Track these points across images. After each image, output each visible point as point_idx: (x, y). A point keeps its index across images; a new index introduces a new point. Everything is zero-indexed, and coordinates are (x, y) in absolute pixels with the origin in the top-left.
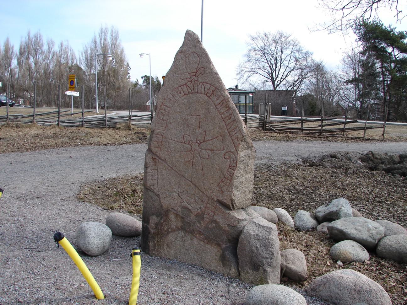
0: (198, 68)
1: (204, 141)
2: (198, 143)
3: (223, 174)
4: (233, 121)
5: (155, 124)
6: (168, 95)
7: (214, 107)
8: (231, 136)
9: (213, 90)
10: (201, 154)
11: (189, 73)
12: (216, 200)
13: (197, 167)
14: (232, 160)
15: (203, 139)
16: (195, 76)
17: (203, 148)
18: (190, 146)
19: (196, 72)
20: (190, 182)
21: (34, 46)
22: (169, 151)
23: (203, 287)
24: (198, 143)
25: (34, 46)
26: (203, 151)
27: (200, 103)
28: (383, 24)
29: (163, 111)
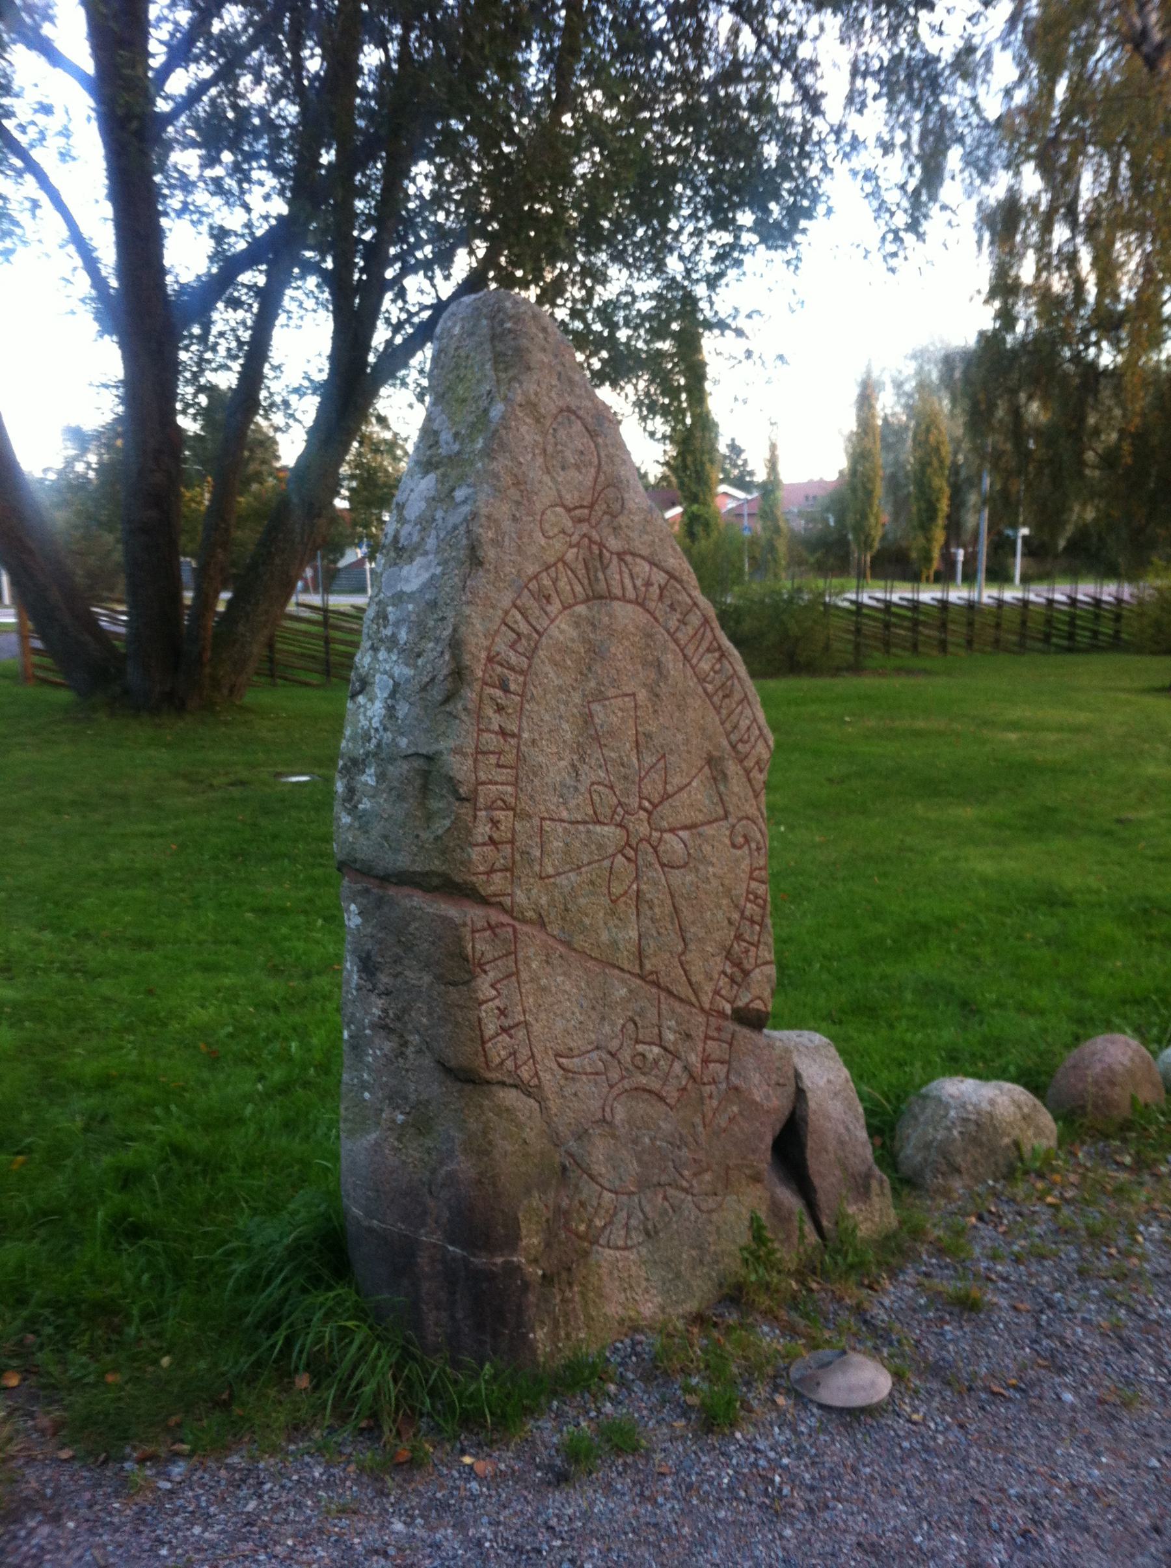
0: (599, 488)
1: (666, 797)
2: (645, 810)
3: (736, 906)
4: (741, 702)
5: (476, 761)
6: (506, 613)
7: (675, 654)
8: (741, 759)
9: (662, 582)
10: (666, 852)
11: (569, 510)
12: (729, 1012)
13: (657, 910)
14: (753, 845)
15: (660, 787)
16: (588, 520)
17: (665, 824)
18: (618, 830)
19: (591, 507)
20: (638, 982)
21: (342, 648)
22: (551, 871)
23: (909, 1421)
24: (645, 810)
25: (342, 648)
26: (667, 836)
27: (627, 643)
28: (914, 357)
29: (498, 693)
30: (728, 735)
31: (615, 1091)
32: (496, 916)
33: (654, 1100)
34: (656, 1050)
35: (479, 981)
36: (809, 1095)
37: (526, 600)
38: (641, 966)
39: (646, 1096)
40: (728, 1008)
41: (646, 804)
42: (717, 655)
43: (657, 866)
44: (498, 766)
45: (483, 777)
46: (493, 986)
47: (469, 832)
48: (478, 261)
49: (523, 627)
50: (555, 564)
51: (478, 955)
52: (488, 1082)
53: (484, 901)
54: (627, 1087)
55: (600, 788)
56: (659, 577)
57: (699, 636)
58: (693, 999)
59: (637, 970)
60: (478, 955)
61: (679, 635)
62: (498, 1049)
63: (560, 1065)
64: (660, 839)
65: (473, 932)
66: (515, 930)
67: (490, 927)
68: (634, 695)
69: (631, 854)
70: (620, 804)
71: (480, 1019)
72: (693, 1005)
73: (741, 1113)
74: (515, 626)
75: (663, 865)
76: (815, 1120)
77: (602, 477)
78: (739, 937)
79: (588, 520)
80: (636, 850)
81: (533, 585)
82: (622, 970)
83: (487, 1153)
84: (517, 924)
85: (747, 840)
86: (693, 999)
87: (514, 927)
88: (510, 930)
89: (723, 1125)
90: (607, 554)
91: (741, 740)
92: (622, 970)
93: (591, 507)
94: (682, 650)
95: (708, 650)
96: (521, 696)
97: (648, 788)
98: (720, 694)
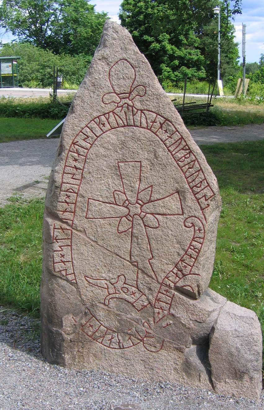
11: (118, 94)
14: (197, 228)
22: (91, 216)
30: (189, 183)
31: (111, 296)
32: (64, 226)
33: (130, 305)
34: (134, 289)
35: (54, 244)
36: (215, 331)
37: (93, 125)
38: (131, 258)
39: (126, 302)
40: (172, 285)
41: (140, 202)
42: (188, 151)
43: (142, 225)
44: (72, 178)
45: (65, 181)
46: (60, 247)
47: (57, 198)
48: (206, 73)
49: (90, 134)
50: (108, 113)
51: (55, 236)
52: (55, 276)
53: (61, 220)
54: (117, 297)
55: (118, 192)
56: (160, 119)
57: (177, 143)
58: (154, 276)
59: (128, 259)
60: (55, 236)
61: (167, 142)
62: (59, 267)
63: (86, 279)
64: (145, 216)
65: (54, 228)
66: (72, 232)
67: (61, 228)
68: (140, 162)
69: (131, 219)
70: (127, 200)
71: (53, 256)
72: (153, 278)
73: (174, 324)
74: (86, 134)
75: (145, 226)
76: (212, 342)
77: (136, 83)
78: (182, 260)
79: (128, 98)
80: (133, 218)
81: (97, 120)
82: (121, 257)
83: (53, 296)
84: (72, 230)
85: (193, 225)
86: (154, 276)
87: (71, 230)
88: (70, 231)
89: (163, 325)
90: (136, 110)
91: (196, 186)
92: (121, 257)
93: (130, 93)
94: (168, 148)
95: (183, 149)
96: (86, 157)
97: (141, 196)
98: (187, 167)
